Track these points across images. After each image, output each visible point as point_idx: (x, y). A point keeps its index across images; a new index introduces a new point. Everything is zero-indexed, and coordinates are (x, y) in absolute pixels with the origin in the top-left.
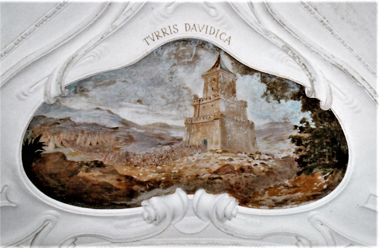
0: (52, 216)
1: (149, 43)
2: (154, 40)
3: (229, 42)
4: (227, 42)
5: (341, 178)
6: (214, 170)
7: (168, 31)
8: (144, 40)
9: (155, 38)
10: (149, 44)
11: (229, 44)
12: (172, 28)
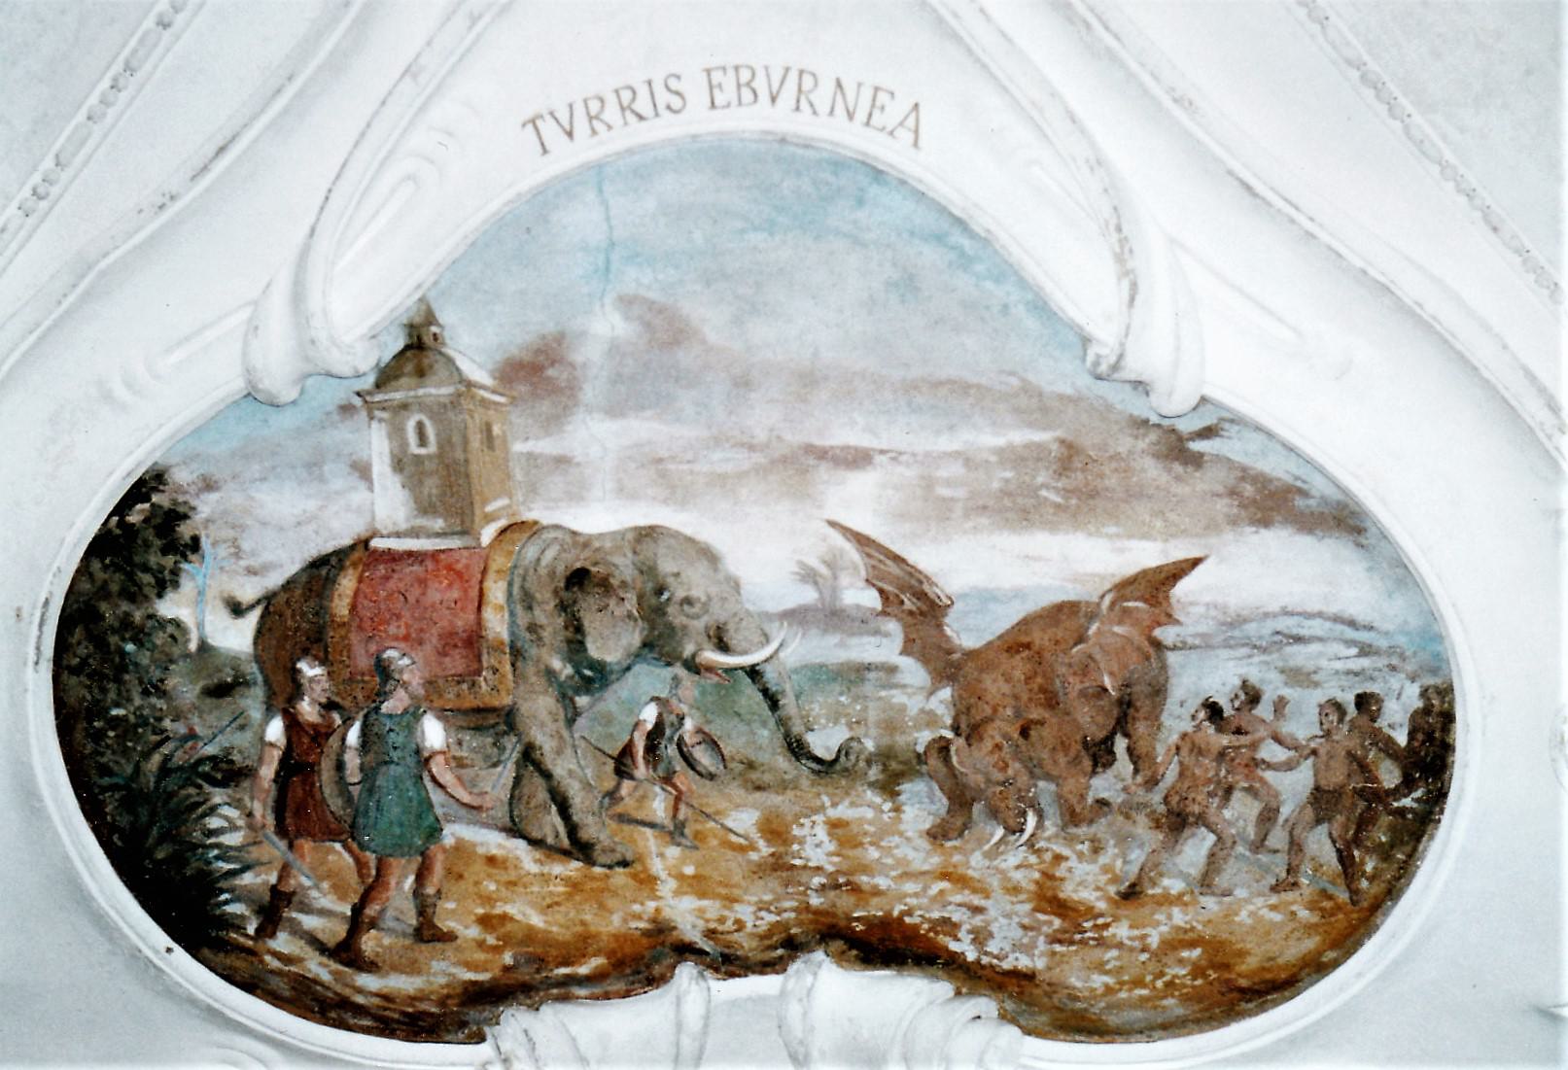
0: (352, 1021)
1: (548, 148)
2: (570, 134)
3: (916, 132)
4: (905, 136)
5: (1216, 850)
6: (679, 849)
7: (643, 105)
8: (530, 127)
9: (581, 126)
10: (545, 151)
11: (916, 144)
12: (659, 88)
